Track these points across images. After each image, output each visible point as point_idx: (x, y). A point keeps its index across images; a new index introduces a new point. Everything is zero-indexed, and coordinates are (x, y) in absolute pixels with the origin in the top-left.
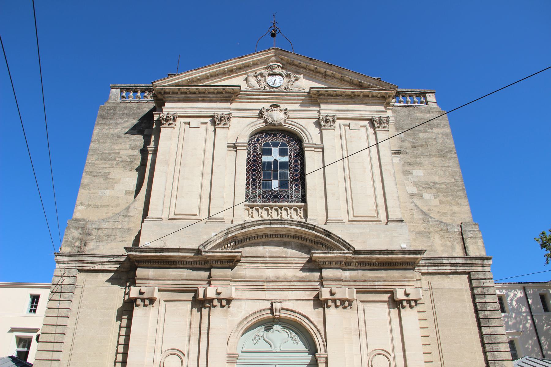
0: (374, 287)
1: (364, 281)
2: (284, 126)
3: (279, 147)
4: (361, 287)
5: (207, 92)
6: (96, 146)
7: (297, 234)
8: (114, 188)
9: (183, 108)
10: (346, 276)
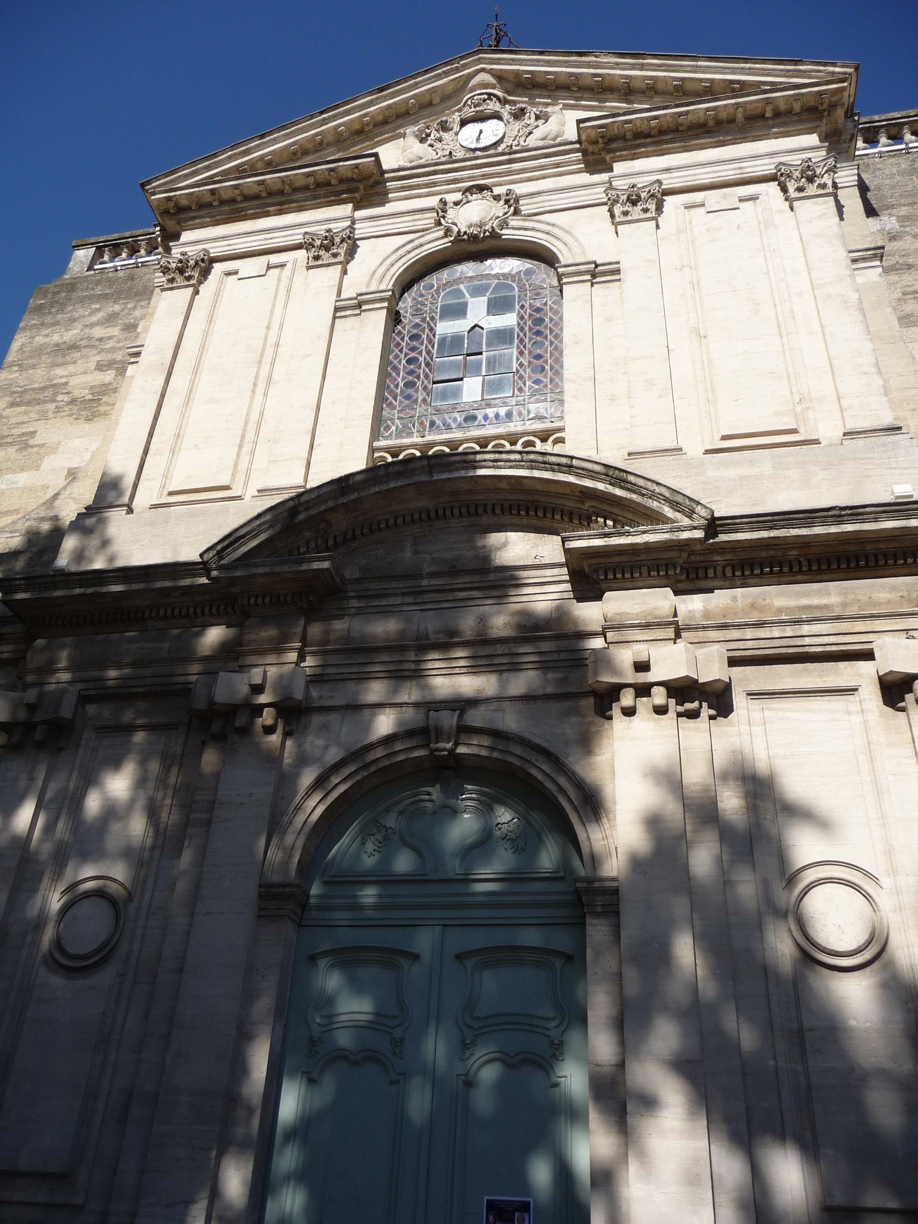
0: (799, 642)
1: (759, 625)
2: (503, 237)
3: (490, 295)
4: (750, 644)
5: (287, 187)
6: (12, 376)
7: (522, 497)
8: (39, 466)
9: (224, 238)
10: (689, 612)
